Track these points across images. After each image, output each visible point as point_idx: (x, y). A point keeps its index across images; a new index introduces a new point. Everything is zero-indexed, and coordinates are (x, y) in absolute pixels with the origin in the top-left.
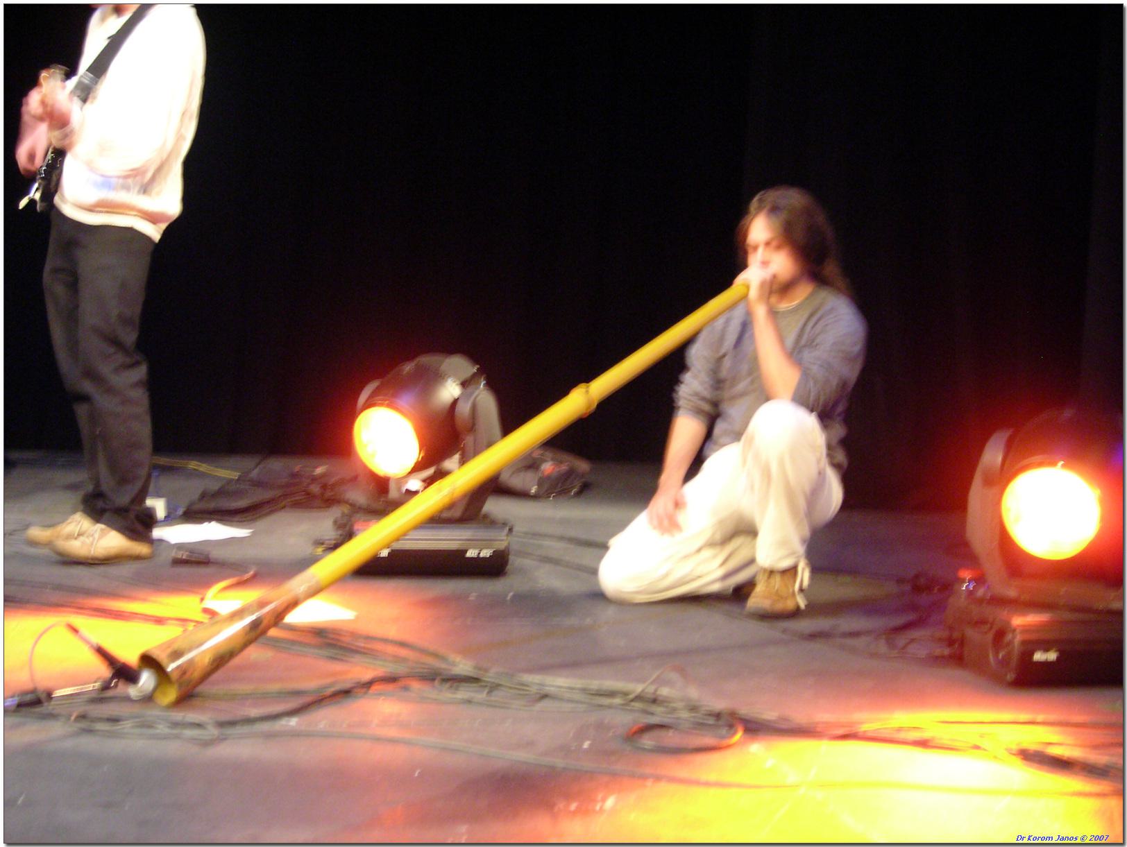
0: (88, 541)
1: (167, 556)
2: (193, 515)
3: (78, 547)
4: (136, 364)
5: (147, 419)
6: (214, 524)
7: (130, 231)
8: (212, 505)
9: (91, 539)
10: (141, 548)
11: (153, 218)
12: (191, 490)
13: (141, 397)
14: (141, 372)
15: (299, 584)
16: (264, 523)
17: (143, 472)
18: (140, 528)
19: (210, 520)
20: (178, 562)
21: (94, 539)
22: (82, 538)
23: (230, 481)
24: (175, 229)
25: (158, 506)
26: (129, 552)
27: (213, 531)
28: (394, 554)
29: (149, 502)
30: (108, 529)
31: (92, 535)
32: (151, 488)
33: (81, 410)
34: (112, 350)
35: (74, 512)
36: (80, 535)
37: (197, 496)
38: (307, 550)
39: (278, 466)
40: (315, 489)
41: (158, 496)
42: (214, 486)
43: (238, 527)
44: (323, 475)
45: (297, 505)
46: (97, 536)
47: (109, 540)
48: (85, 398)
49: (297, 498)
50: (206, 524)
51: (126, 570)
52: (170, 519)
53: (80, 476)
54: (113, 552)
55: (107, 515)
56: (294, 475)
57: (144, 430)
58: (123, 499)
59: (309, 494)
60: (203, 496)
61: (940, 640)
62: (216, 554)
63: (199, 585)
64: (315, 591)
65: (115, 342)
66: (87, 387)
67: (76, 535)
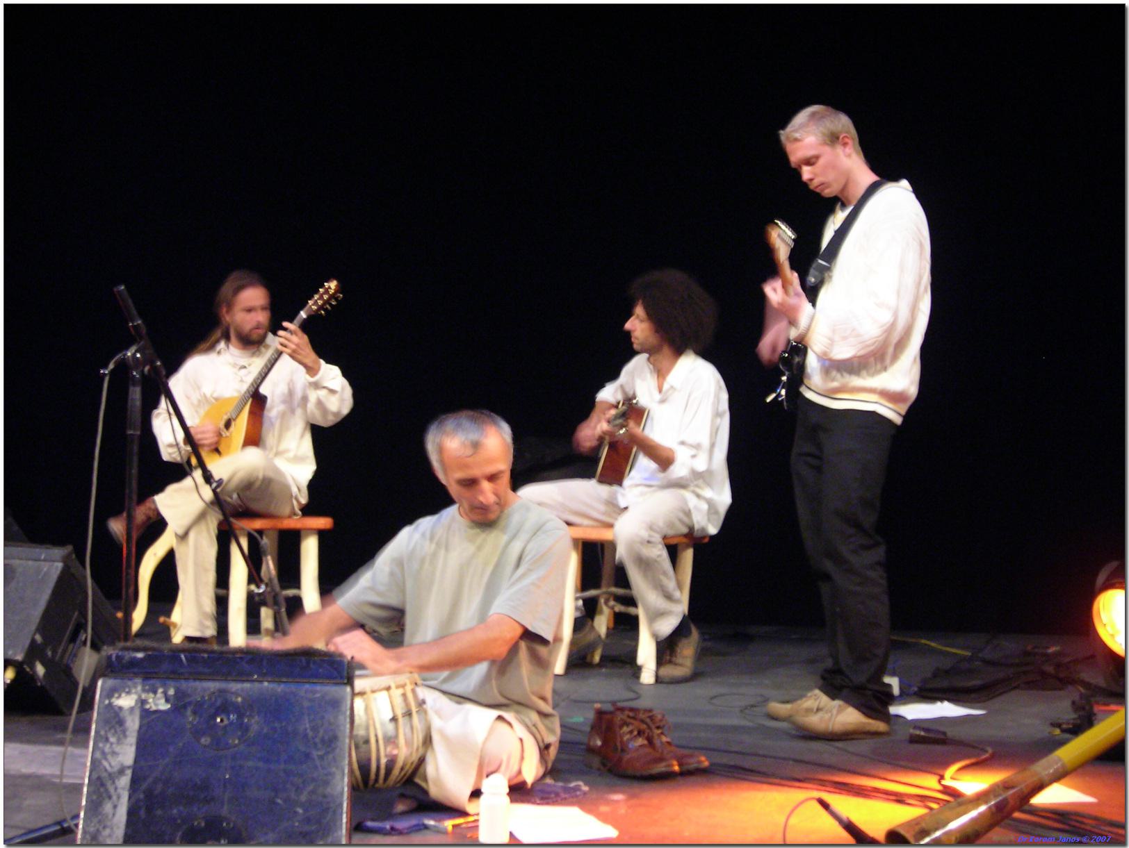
0: (827, 716)
1: (903, 733)
2: (927, 694)
3: (816, 721)
4: (876, 545)
5: (885, 599)
6: (946, 703)
7: (873, 414)
8: (945, 684)
9: (830, 714)
10: (880, 726)
11: (894, 397)
12: (924, 667)
13: (877, 575)
14: (879, 553)
15: (1043, 767)
16: (997, 703)
17: (880, 651)
18: (878, 707)
19: (942, 700)
20: (914, 740)
21: (832, 715)
22: (820, 714)
23: (964, 659)
24: (919, 410)
25: (893, 682)
26: (867, 728)
27: (946, 709)
28: (188, 428)
29: (887, 680)
30: (846, 705)
31: (831, 711)
32: (890, 666)
33: (825, 588)
34: (851, 531)
35: (810, 689)
36: (818, 710)
37: (929, 675)
38: (1044, 731)
39: (1010, 646)
40: (1050, 669)
41: (893, 674)
42: (947, 664)
43: (963, 706)
44: (1055, 654)
45: (1031, 685)
46: (835, 712)
47: (848, 716)
48: (827, 577)
49: (933, 644)
50: (939, 704)
51: (864, 746)
52: (908, 696)
53: (822, 650)
54: (850, 728)
55: (845, 691)
56: (1026, 654)
57: (881, 609)
58: (860, 679)
59: (1043, 674)
60: (936, 674)
61: (230, 364)
62: (951, 732)
63: (936, 765)
64: (1058, 777)
65: (858, 526)
66: (829, 566)
67: (815, 710)
